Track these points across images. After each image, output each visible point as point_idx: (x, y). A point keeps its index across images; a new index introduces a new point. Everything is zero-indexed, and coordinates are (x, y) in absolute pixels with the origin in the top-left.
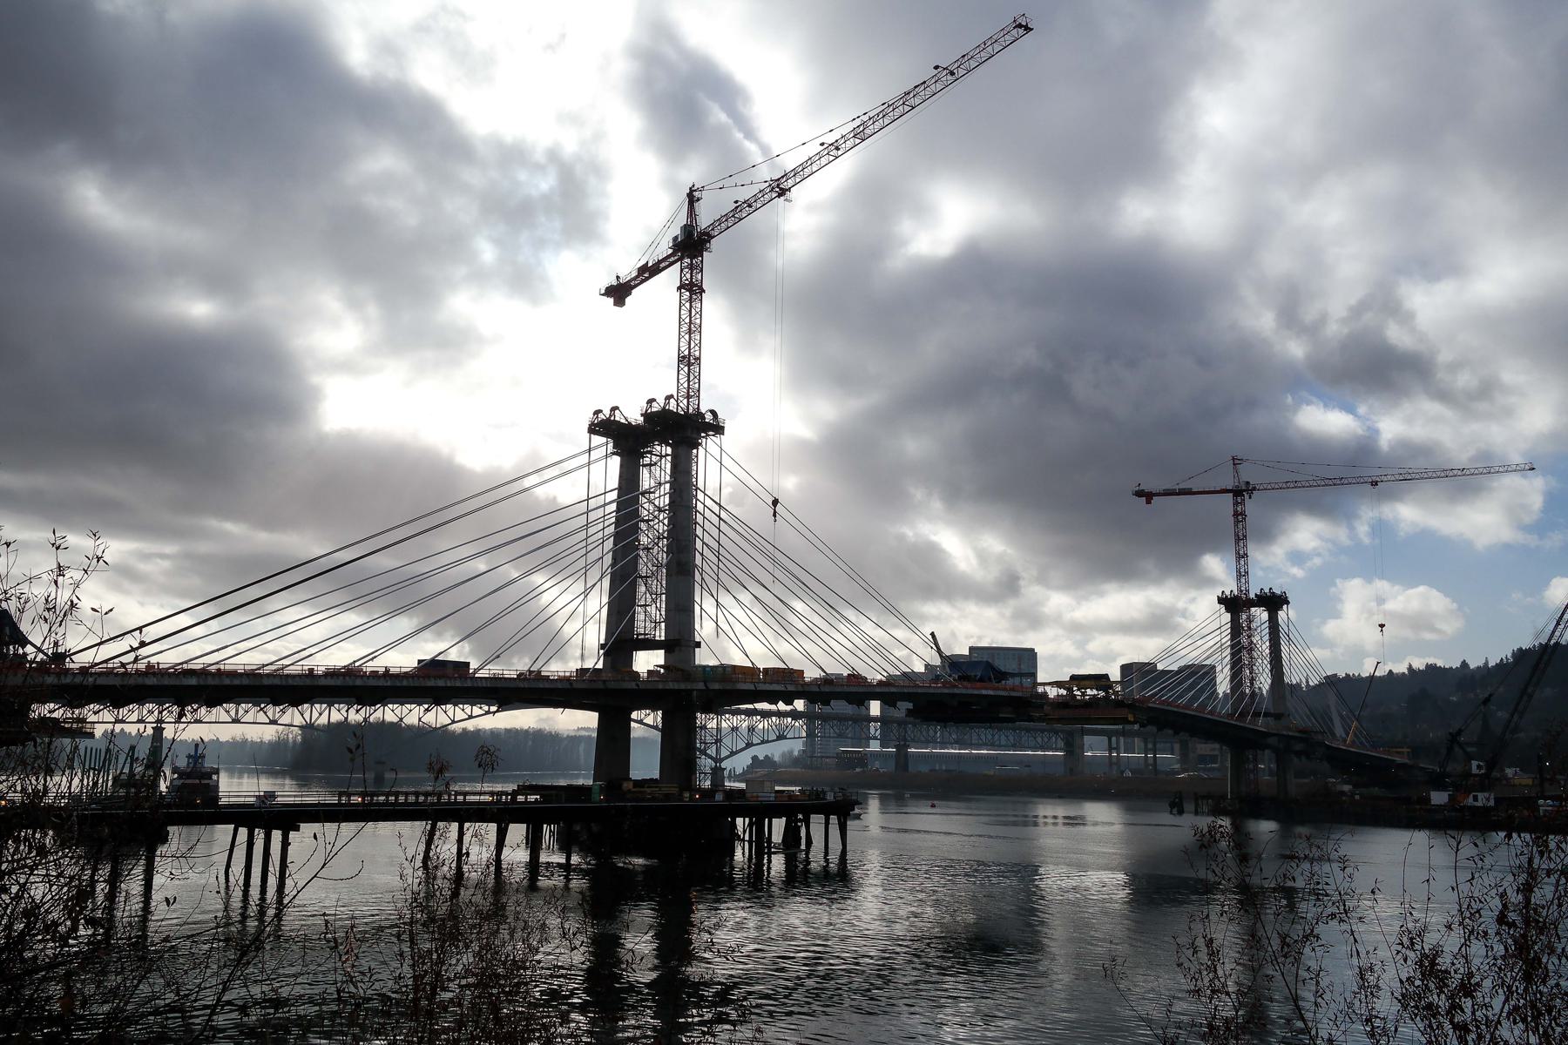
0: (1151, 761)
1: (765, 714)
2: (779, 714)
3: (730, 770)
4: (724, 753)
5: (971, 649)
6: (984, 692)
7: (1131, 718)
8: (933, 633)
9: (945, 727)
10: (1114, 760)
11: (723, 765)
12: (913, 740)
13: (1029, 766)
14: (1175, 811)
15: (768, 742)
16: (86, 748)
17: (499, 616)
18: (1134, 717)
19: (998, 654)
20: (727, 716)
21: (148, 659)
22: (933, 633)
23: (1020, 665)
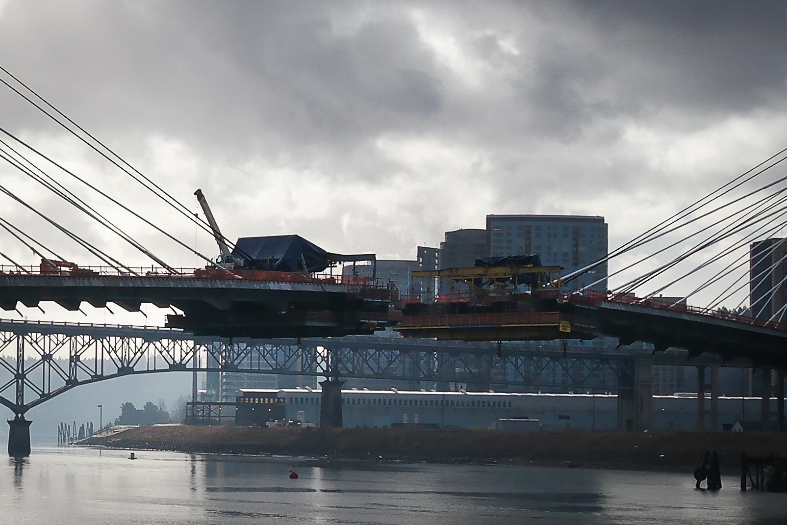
0: (774, 409)
1: (98, 333)
2: (125, 332)
3: (82, 428)
4: (30, 396)
5: (490, 219)
6: (272, 286)
7: (565, 327)
8: (199, 191)
9: (231, 344)
10: (707, 407)
11: (27, 416)
12: (351, 374)
13: (567, 418)
14: (704, 485)
15: (101, 378)
16: (62, 424)
17: (771, 207)
18: (572, 326)
19: (538, 228)
20: (34, 335)
21: (660, 293)
22: (199, 191)
23: (576, 246)
